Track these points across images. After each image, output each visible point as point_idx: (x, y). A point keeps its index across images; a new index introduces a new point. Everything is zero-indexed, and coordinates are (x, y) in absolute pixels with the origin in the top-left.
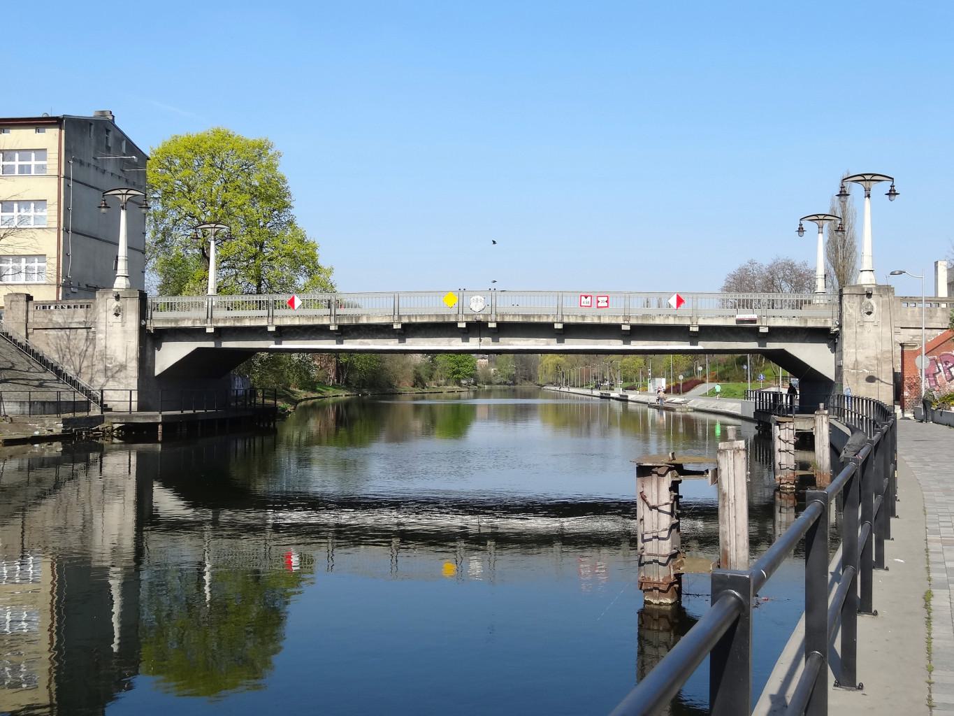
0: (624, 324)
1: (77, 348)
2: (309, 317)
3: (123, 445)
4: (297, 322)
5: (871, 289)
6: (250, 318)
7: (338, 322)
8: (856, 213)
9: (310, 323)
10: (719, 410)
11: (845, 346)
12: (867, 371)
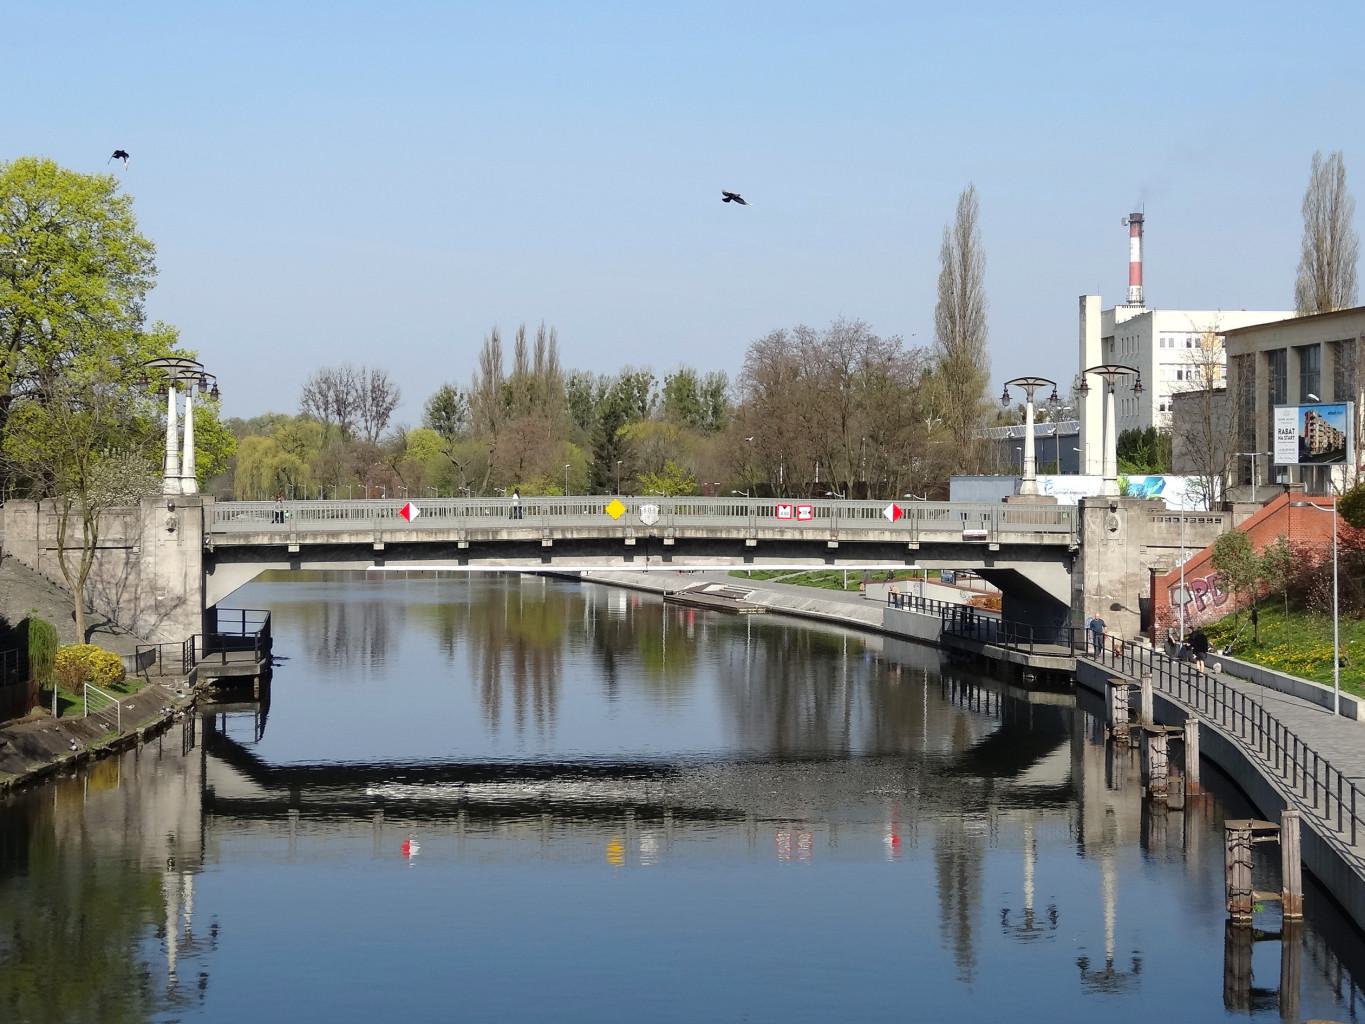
0: (831, 541)
1: (112, 576)
2: (430, 532)
3: (218, 706)
4: (413, 538)
5: (1116, 502)
6: (352, 533)
7: (469, 539)
8: (984, 258)
9: (432, 539)
10: (822, 614)
11: (1087, 568)
12: (1110, 597)
